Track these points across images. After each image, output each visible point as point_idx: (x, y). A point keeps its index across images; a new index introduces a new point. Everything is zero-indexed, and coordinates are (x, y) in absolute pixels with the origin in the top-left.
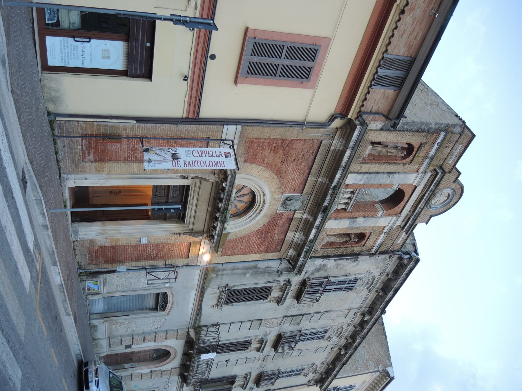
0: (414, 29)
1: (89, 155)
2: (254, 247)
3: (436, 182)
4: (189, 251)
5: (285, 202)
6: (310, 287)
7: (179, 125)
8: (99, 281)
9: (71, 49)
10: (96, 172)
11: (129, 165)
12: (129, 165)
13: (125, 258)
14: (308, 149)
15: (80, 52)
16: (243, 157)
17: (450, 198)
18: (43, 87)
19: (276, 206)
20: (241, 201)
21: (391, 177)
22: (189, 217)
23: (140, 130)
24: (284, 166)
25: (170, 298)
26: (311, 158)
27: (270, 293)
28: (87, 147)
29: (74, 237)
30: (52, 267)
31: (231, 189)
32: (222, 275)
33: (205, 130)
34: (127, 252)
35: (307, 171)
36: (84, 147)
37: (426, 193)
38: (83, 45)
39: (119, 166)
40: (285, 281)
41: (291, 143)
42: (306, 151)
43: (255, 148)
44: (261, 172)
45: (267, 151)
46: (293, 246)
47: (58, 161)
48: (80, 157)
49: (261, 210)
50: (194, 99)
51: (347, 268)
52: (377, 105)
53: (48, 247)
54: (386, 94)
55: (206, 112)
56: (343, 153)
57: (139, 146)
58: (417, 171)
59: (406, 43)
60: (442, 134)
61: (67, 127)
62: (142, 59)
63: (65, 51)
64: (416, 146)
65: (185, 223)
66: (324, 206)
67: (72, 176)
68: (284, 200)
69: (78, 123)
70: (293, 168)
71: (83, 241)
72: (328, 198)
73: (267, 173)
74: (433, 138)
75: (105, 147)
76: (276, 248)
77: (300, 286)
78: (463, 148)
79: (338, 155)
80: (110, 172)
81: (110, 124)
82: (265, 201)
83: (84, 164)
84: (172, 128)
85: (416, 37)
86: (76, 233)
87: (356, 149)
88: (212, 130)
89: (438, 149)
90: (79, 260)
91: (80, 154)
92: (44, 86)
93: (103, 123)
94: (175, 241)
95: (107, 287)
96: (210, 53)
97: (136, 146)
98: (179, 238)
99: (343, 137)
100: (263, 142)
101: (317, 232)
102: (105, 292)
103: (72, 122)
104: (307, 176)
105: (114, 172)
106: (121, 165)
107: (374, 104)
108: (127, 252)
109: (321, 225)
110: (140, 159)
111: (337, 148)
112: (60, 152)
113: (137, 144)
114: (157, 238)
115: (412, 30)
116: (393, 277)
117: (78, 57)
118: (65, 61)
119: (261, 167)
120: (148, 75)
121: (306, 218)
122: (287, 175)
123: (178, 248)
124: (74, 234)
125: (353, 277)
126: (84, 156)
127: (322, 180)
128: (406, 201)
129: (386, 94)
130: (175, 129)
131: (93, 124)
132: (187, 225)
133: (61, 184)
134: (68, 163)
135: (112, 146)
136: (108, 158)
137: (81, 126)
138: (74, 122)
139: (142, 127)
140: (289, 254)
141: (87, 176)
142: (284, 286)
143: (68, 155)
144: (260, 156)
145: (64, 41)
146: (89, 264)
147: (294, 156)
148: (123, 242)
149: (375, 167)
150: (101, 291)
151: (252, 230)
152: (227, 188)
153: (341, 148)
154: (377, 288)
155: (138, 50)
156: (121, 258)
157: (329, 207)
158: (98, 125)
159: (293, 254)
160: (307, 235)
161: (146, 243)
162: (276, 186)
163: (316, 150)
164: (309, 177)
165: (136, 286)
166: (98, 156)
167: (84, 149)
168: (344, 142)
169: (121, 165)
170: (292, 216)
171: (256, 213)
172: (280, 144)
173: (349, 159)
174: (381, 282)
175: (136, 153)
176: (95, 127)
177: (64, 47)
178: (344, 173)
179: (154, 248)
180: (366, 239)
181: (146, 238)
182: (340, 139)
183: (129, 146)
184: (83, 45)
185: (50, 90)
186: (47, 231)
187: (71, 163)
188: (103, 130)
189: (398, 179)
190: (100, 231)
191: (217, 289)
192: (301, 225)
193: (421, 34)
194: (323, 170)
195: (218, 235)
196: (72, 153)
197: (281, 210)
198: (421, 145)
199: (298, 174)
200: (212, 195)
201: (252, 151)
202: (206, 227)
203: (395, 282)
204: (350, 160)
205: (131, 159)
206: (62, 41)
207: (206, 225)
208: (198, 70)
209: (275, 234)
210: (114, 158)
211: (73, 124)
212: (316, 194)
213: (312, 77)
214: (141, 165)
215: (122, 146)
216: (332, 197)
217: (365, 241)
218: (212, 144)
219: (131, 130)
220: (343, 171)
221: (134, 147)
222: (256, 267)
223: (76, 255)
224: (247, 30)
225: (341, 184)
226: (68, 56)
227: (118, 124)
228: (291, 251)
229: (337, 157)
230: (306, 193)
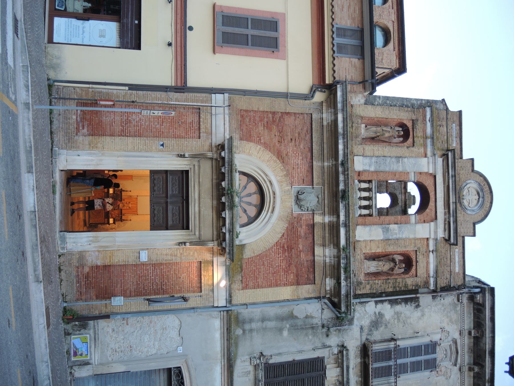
0: (350, 4)
2: (281, 274)
3: (452, 165)
4: (201, 273)
5: (298, 198)
6: (376, 361)
7: (169, 93)
8: (88, 336)
9: (74, 29)
10: (89, 148)
11: (123, 141)
12: (123, 141)
13: (122, 290)
14: (302, 126)
15: (81, 32)
16: (237, 132)
17: (481, 196)
18: (46, 54)
20: (249, 195)
21: (400, 162)
23: (132, 97)
24: (283, 147)
25: (187, 380)
26: (307, 138)
27: (324, 371)
28: (81, 119)
29: (61, 244)
30: (27, 175)
31: (231, 157)
32: (251, 330)
33: (195, 100)
34: (124, 279)
35: (309, 154)
36: (78, 119)
37: (449, 182)
38: (84, 25)
39: (112, 142)
40: (338, 346)
41: (282, 117)
42: (300, 128)
43: (248, 123)
45: (261, 128)
46: (328, 272)
47: (51, 133)
48: (74, 129)
49: (274, 208)
50: (180, 66)
51: (412, 320)
52: (349, 74)
53: (26, 139)
54: (353, 63)
56: (336, 121)
57: (132, 118)
59: (349, 16)
60: (428, 110)
61: (64, 93)
62: (131, 34)
63: (68, 31)
64: (409, 125)
65: (190, 229)
66: (341, 191)
67: (65, 151)
68: (295, 194)
69: (74, 89)
70: (293, 149)
71: (71, 253)
72: (341, 178)
73: (267, 155)
74: (421, 114)
75: (99, 118)
76: (308, 278)
77: (362, 360)
78: (458, 128)
79: (333, 127)
80: (103, 148)
81: (105, 90)
82: (274, 194)
83: (77, 138)
84: (162, 96)
85: (354, 11)
86: (63, 240)
87: (345, 109)
88: (201, 100)
89: (432, 126)
90: (64, 293)
91: (74, 125)
92: (47, 53)
93: (98, 90)
94: (181, 258)
95: (99, 351)
97: (129, 118)
98: (185, 254)
99: (330, 107)
100: (254, 116)
101: (346, 232)
102: (96, 364)
103: (69, 88)
104: (311, 161)
105: (108, 149)
106: (114, 140)
107: (346, 73)
108: (124, 279)
109: (347, 218)
110: (134, 134)
111: (329, 121)
112: (55, 122)
113: (131, 115)
114: (159, 253)
115: (348, 5)
116: (478, 333)
117: (79, 36)
118: (68, 39)
119: (259, 147)
120: (138, 47)
121: (330, 222)
122: (290, 160)
123: (187, 274)
124: (61, 241)
125: (426, 340)
126: (78, 129)
127: (328, 164)
128: (434, 199)
129: (353, 63)
130: (165, 98)
131: (88, 91)
132: (193, 233)
133: (52, 160)
134: (61, 137)
135: (106, 118)
136: (101, 132)
137: (77, 92)
138: (71, 88)
139: (134, 95)
140: (328, 288)
141: (80, 152)
142: (340, 355)
143: (62, 126)
145: (69, 21)
146: (77, 300)
147: (289, 134)
148: (118, 259)
150: (91, 359)
152: (226, 158)
153: (333, 118)
154: (468, 364)
155: (129, 26)
156: (117, 290)
157: (347, 191)
158: (92, 91)
159: (333, 285)
160: (337, 244)
161: (146, 260)
162: (282, 174)
163: (309, 128)
164: (314, 161)
165: (138, 352)
166: (92, 130)
167: (78, 121)
168: (333, 110)
169: (114, 140)
170: (312, 220)
172: (271, 119)
173: (344, 122)
174: (468, 352)
175: (130, 127)
176: (90, 94)
177: (68, 27)
179: (157, 273)
180: (414, 263)
181: (146, 251)
182: (328, 110)
183: (122, 118)
184: (84, 25)
185: (53, 57)
186: (28, 113)
187: (64, 136)
188: (97, 97)
189: (410, 166)
191: (248, 363)
192: (327, 235)
193: (357, 8)
194: (325, 151)
195: (230, 231)
196: (67, 123)
197: (297, 211)
200: (214, 181)
201: (245, 126)
202: (215, 233)
203: (484, 338)
204: (346, 124)
205: (125, 135)
206: (67, 22)
208: (180, 38)
210: (108, 133)
211: (70, 91)
212: (329, 184)
213: (280, 47)
214: (135, 141)
215: (116, 118)
216: (345, 174)
217: (414, 268)
218: (203, 116)
220: (344, 138)
221: (128, 119)
222: (291, 316)
223: (61, 280)
224: (214, 6)
225: (347, 155)
226: (71, 35)
227: (111, 91)
228: (328, 280)
229: (333, 129)
230: (318, 184)
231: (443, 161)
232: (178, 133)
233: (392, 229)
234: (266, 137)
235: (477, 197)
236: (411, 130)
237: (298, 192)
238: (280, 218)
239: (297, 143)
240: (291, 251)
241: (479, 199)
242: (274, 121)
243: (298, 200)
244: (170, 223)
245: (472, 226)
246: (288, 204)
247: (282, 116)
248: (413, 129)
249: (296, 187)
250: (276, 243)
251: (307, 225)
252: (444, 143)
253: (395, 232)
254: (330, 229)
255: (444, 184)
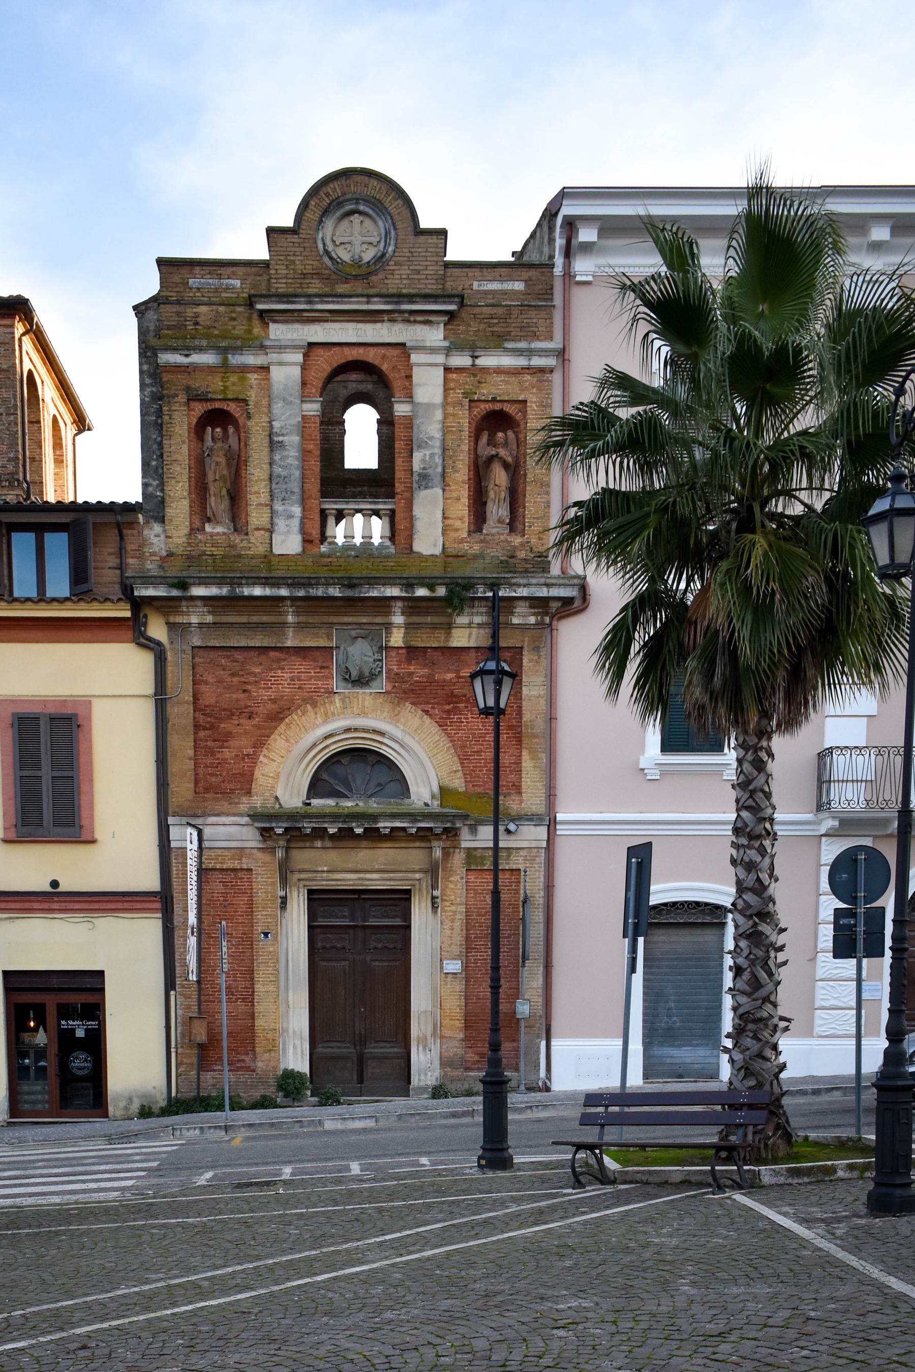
1: (243, 1061)
7: (176, 923)
16: (237, 800)
17: (352, 207)
19: (367, 698)
21: (281, 439)
22: (392, 883)
26: (239, 657)
35: (272, 654)
41: (203, 710)
43: (220, 779)
44: (272, 755)
45: (227, 753)
49: (375, 731)
55: (150, 881)
58: (265, 369)
64: (199, 409)
68: (350, 685)
69: (181, 1075)
70: (264, 688)
73: (277, 742)
78: (197, 270)
82: (348, 730)
96: (50, 889)
99: (176, 607)
119: (261, 758)
121: (403, 614)
122: (283, 696)
128: (361, 350)
131: (181, 1054)
132: (417, 882)
144: (237, 766)
147: (234, 696)
149: (256, 493)
151: (438, 738)
152: (285, 825)
161: (460, 962)
164: (286, 645)
171: (386, 741)
178: (244, 582)
180: (497, 406)
190: (421, 1048)
194: (265, 619)
195: (416, 821)
197: (382, 684)
198: (194, 397)
199: (279, 673)
202: (417, 844)
207: (412, 845)
209: (460, 677)
212: (329, 614)
217: (507, 408)
219: (190, 998)
220: (240, 585)
227: (179, 1018)
231: (275, 321)
232: (243, 908)
233: (422, 466)
234: (242, 744)
235: (356, 218)
236: (209, 406)
237: (346, 679)
238: (395, 718)
239: (252, 679)
240: (456, 696)
241: (360, 213)
242: (212, 727)
243: (361, 681)
244: (398, 922)
245: (422, 239)
246: (368, 701)
247: (201, 710)
248: (207, 400)
249: (335, 683)
250: (440, 726)
251: (409, 661)
252: (234, 315)
253: (427, 458)
254: (418, 614)
255: (327, 321)
